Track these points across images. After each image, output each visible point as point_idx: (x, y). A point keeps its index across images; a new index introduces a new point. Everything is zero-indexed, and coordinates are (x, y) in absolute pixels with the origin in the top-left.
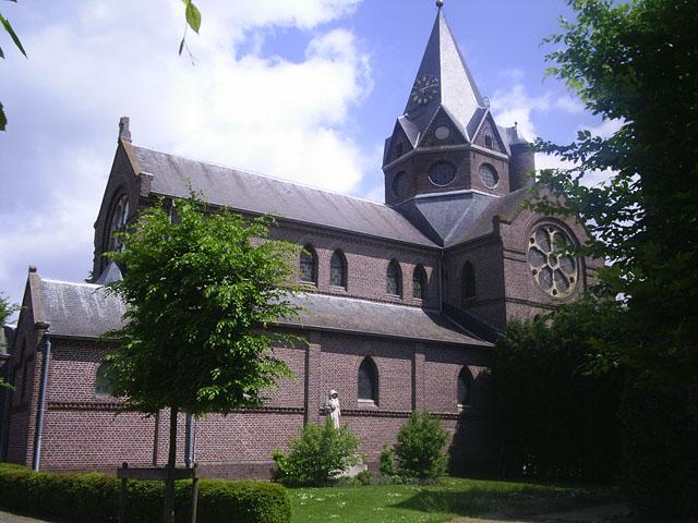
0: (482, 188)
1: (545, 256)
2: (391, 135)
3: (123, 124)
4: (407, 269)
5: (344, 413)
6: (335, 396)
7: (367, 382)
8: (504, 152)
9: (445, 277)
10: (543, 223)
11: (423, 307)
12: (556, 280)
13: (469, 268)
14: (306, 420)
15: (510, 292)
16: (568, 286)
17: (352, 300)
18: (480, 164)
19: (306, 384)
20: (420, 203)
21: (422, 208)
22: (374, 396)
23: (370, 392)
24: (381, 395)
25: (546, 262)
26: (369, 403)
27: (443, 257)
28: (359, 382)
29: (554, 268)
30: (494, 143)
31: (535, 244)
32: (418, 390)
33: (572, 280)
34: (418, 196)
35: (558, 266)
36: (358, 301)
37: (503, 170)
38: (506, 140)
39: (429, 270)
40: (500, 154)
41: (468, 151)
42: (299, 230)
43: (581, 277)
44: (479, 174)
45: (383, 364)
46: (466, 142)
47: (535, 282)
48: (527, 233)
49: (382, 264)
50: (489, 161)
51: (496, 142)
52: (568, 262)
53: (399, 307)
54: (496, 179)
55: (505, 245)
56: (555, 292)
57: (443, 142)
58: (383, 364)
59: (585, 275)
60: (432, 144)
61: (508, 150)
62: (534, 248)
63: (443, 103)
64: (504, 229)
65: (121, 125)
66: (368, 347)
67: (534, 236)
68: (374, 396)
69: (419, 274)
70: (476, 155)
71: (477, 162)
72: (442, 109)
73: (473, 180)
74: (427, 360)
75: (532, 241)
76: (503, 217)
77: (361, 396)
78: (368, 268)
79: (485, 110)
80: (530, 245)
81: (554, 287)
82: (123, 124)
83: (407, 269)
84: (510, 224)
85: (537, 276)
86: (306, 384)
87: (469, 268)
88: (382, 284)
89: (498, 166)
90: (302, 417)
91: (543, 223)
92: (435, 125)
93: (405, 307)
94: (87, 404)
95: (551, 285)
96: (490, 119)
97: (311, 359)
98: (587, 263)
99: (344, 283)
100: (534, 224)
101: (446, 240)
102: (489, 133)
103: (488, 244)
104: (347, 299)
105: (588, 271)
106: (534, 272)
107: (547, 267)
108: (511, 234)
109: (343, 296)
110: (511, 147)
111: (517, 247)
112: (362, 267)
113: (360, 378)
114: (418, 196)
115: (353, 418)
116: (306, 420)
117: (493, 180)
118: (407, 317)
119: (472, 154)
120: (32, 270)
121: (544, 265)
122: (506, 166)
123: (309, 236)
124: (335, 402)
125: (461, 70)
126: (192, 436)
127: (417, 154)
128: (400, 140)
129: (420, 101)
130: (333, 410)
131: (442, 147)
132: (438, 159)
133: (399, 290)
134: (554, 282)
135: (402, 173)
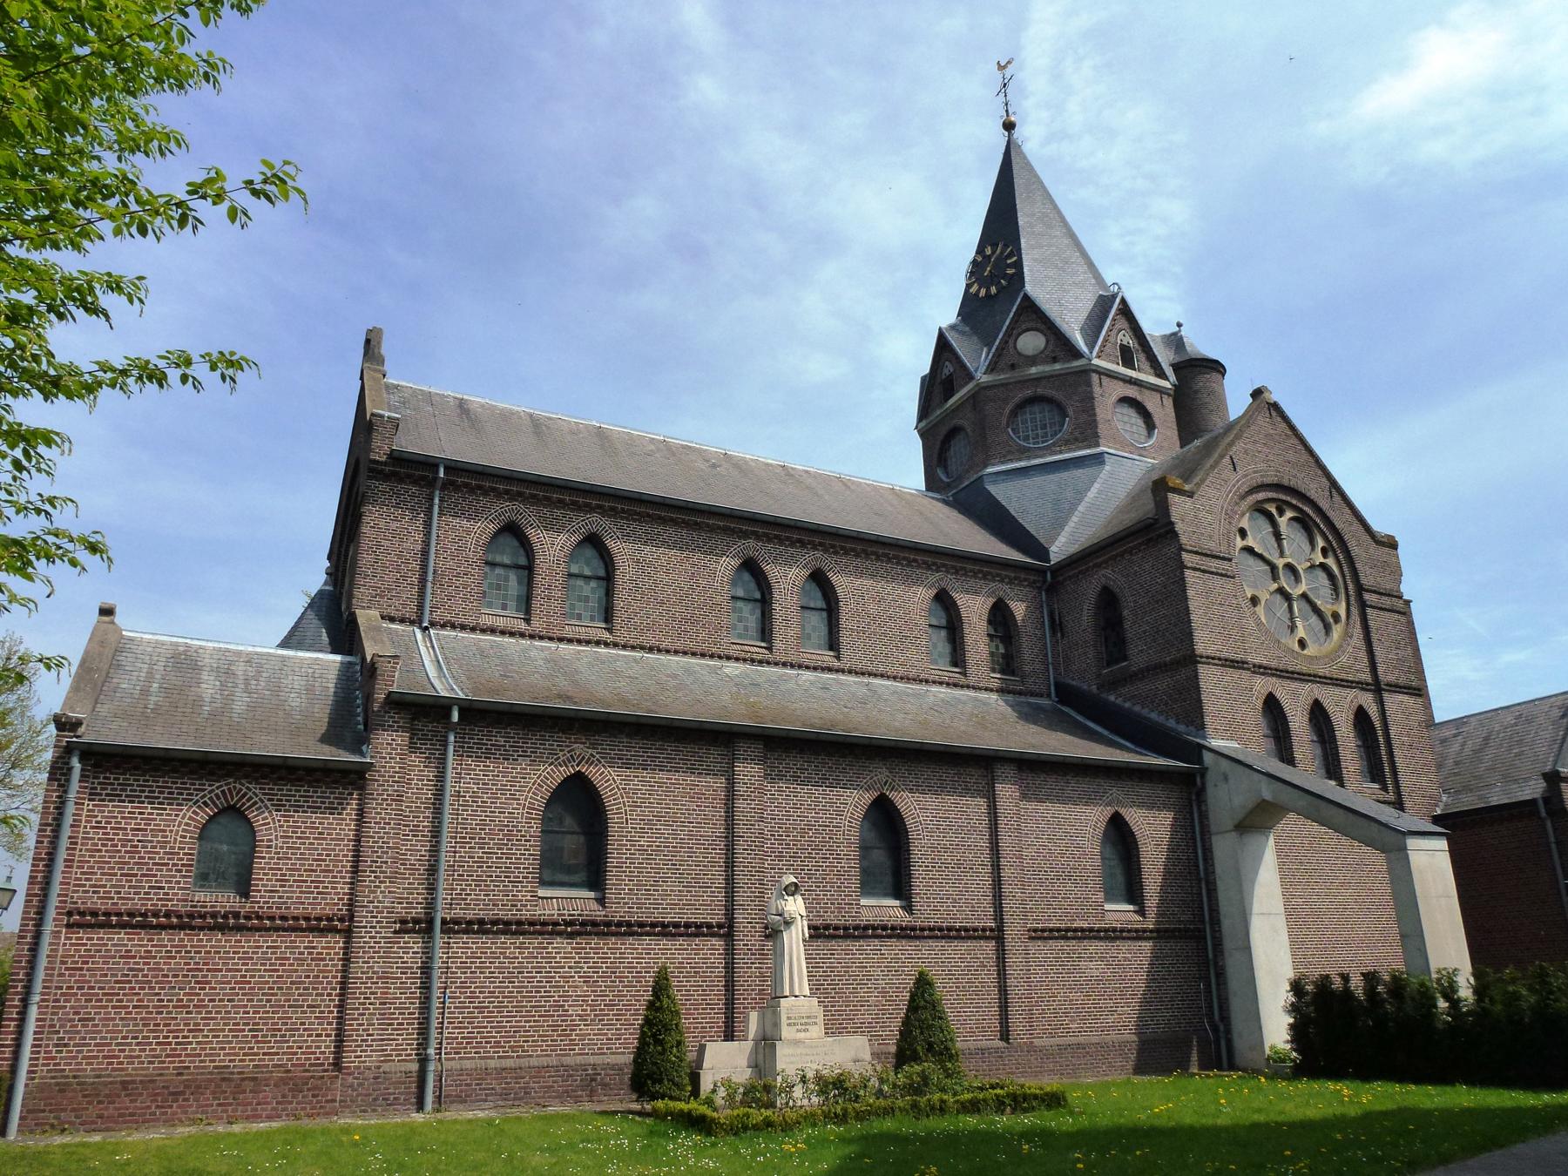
0: (1124, 445)
1: (1273, 568)
2: (927, 370)
3: (371, 347)
4: (974, 607)
5: (818, 932)
6: (792, 890)
7: (880, 856)
8: (1161, 374)
9: (1057, 626)
10: (1261, 496)
11: (1000, 691)
12: (1305, 619)
13: (1109, 601)
14: (730, 952)
15: (1204, 643)
16: (1327, 629)
17: (852, 679)
18: (1114, 398)
19: (730, 865)
20: (995, 482)
21: (1002, 492)
22: (900, 888)
23: (888, 879)
24: (611, 880)
25: (1275, 578)
26: (887, 908)
27: (1050, 580)
28: (863, 857)
29: (1296, 592)
30: (1139, 358)
31: (1250, 542)
32: (1006, 873)
33: (1336, 616)
34: (990, 470)
35: (1303, 587)
36: (866, 680)
37: (1163, 411)
38: (1165, 357)
39: (1019, 609)
40: (1153, 380)
41: (1086, 372)
42: (725, 530)
43: (1355, 611)
44: (1117, 423)
45: (922, 810)
46: (1077, 354)
47: (1259, 624)
48: (1230, 516)
49: (919, 597)
50: (1131, 392)
51: (1142, 357)
52: (1322, 576)
53: (958, 692)
54: (1150, 425)
55: (1184, 539)
56: (1302, 644)
57: (1032, 360)
58: (922, 810)
59: (1363, 605)
60: (1013, 367)
61: (1169, 372)
62: (1249, 550)
63: (1028, 288)
64: (1179, 507)
65: (368, 341)
66: (881, 773)
67: (1245, 523)
68: (900, 888)
69: (999, 616)
70: (1105, 380)
71: (1106, 396)
72: (1027, 297)
73: (1102, 429)
74: (1024, 797)
75: (1243, 533)
76: (1175, 481)
77: (867, 888)
78: (888, 607)
79: (1114, 296)
80: (1239, 543)
81: (1301, 632)
82: (371, 347)
83: (974, 607)
84: (1191, 495)
85: (1260, 610)
86: (730, 865)
87: (1109, 601)
88: (927, 650)
89: (1151, 402)
90: (718, 943)
91: (1261, 496)
92: (1013, 333)
93: (972, 693)
94: (167, 915)
95: (1293, 628)
96: (1126, 312)
97: (740, 804)
98: (1364, 580)
99: (833, 645)
100: (1243, 497)
101: (1053, 549)
102: (1127, 339)
103: (1149, 533)
104: (842, 677)
105: (1367, 596)
106: (1254, 601)
107: (1281, 591)
108: (1200, 516)
109: (830, 670)
110: (1176, 367)
111: (1211, 546)
112: (872, 608)
113: (865, 849)
114: (990, 470)
115: (845, 944)
116: (730, 952)
117: (1145, 433)
118: (975, 712)
119: (1095, 377)
120: (107, 612)
121: (1276, 586)
122: (1168, 402)
123: (751, 542)
124: (795, 906)
125: (1069, 219)
126: (436, 993)
127: (983, 389)
128: (948, 368)
129: (983, 292)
130: (788, 924)
131: (1033, 370)
132: (1029, 393)
133: (958, 658)
134: (1299, 623)
135: (955, 431)
